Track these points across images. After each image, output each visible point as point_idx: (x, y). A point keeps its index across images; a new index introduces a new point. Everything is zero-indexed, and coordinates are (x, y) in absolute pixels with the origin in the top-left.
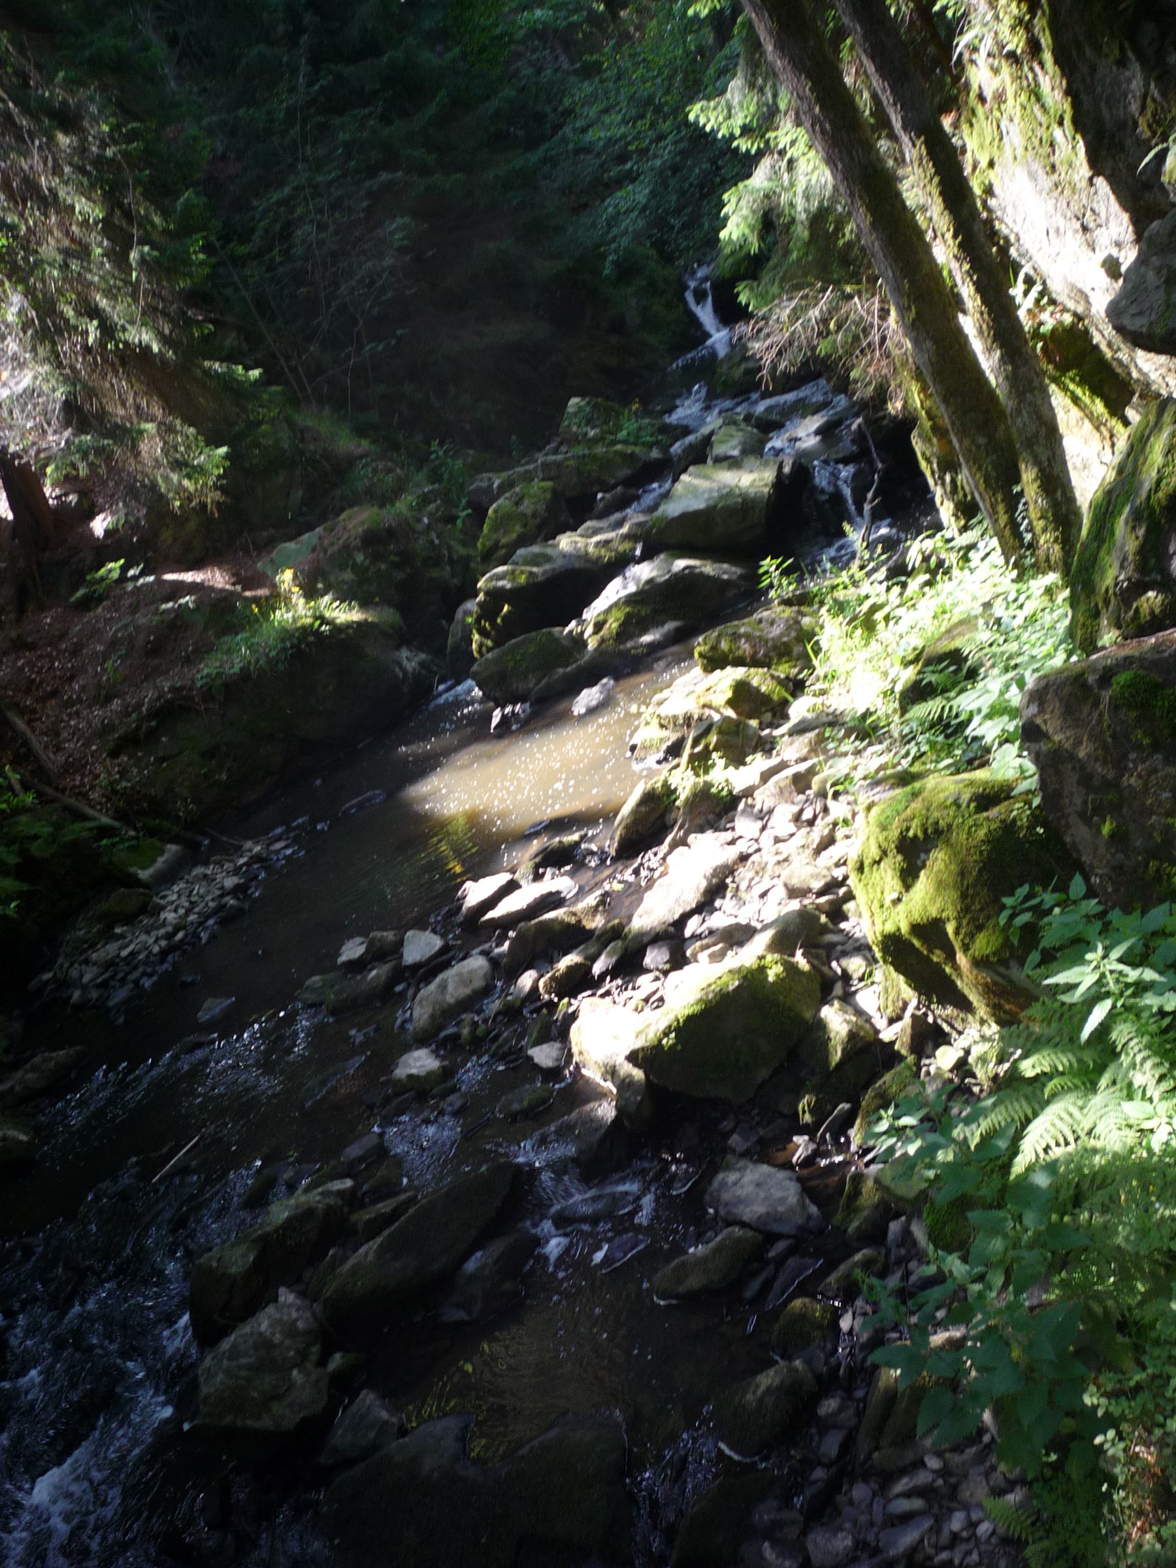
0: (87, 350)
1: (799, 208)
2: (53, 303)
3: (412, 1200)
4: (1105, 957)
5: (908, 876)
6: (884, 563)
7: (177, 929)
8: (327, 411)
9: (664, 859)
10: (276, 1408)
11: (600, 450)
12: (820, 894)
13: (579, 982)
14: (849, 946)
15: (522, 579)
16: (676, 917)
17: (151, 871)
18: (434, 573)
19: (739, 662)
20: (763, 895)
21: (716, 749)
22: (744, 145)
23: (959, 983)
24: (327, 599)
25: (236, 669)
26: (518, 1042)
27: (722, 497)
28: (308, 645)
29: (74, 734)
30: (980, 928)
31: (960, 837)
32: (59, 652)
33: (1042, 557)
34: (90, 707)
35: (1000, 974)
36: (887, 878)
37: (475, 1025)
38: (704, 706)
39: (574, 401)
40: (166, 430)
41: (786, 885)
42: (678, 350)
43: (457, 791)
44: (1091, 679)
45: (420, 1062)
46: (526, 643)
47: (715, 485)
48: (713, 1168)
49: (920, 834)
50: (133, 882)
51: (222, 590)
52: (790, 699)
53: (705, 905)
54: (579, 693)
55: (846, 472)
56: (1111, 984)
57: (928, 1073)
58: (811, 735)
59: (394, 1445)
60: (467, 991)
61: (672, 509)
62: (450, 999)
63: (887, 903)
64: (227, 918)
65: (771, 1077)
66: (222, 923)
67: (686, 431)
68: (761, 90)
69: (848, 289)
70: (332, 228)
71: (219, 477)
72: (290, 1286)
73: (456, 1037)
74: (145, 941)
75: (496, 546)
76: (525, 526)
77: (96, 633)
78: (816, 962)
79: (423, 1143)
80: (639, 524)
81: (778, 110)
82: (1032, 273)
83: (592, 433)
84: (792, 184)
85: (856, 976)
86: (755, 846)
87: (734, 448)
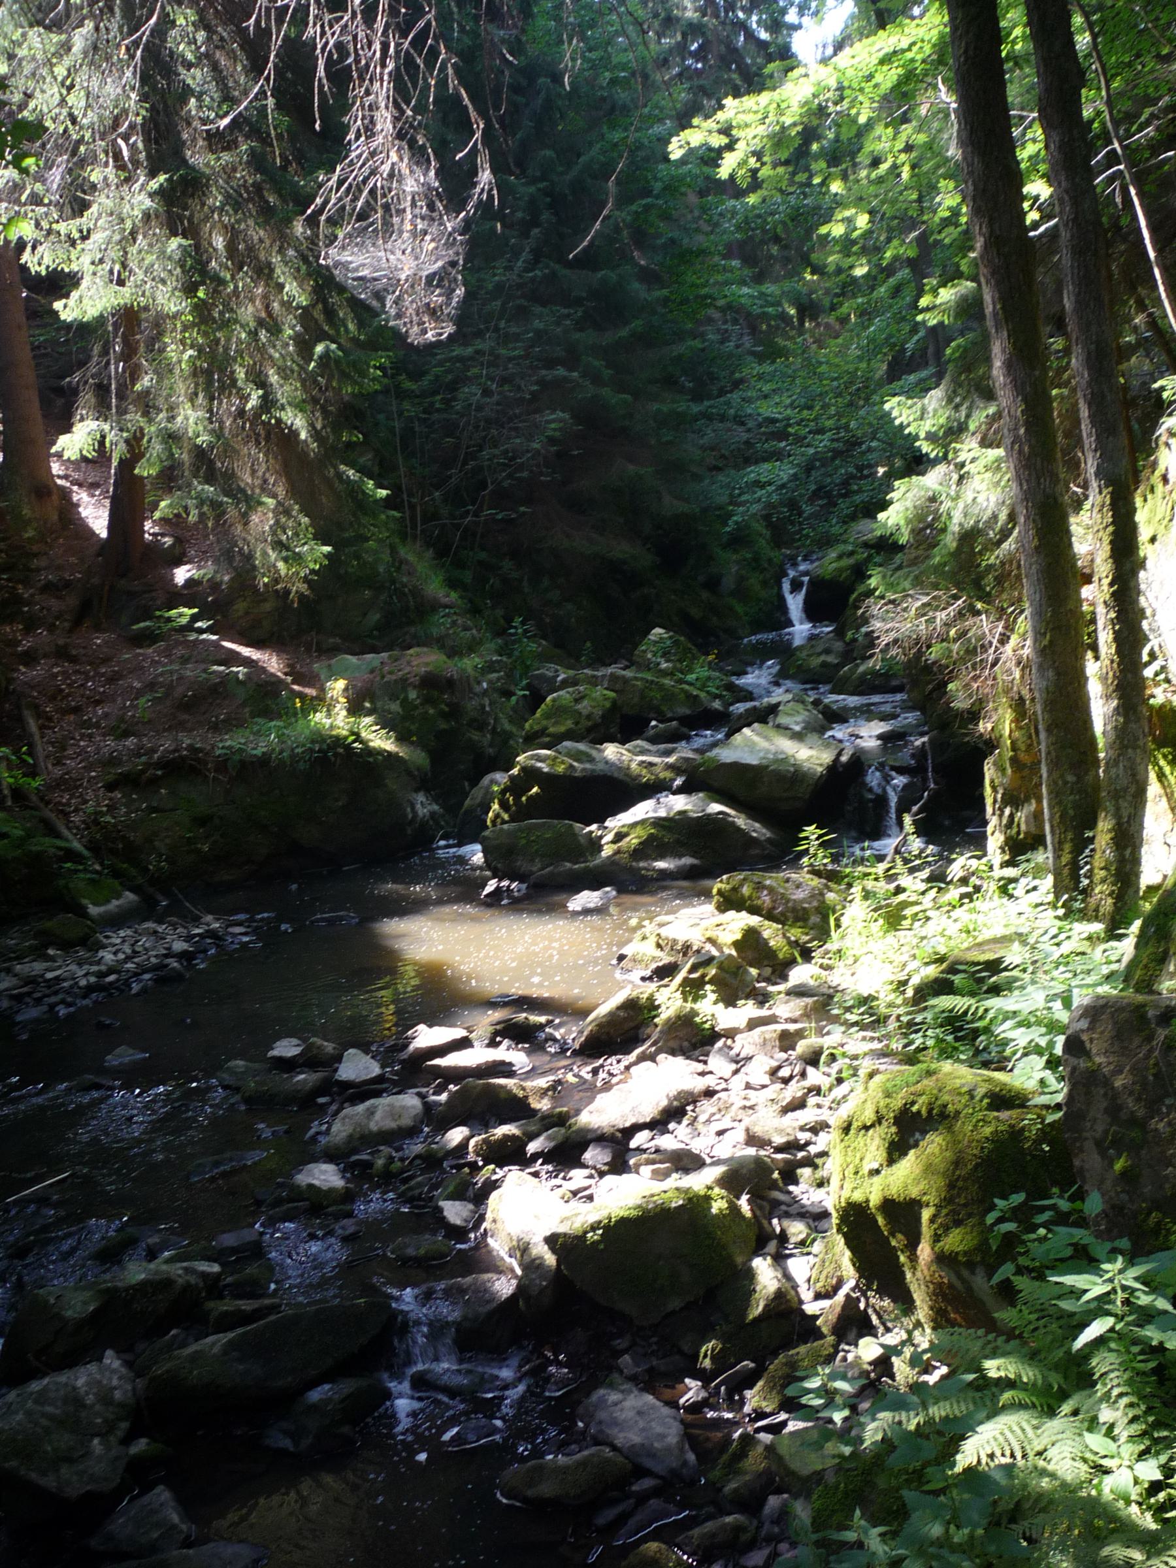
0: (241, 413)
1: (955, 520)
2: (228, 360)
3: (274, 1308)
4: (1121, 1272)
5: (896, 1151)
6: (929, 863)
7: (111, 971)
8: (430, 553)
9: (627, 1068)
10: (64, 1471)
11: (667, 682)
12: (778, 1150)
13: (510, 1154)
14: (793, 1209)
15: (561, 769)
16: (627, 1124)
17: (102, 909)
18: (475, 736)
19: (754, 911)
20: (720, 1133)
21: (711, 982)
22: (925, 447)
23: (909, 1276)
24: (368, 720)
25: (258, 752)
26: (430, 1191)
27: (776, 761)
28: (336, 755)
29: (79, 754)
30: (958, 1223)
31: (964, 1127)
32: (98, 674)
33: (1092, 905)
34: (104, 735)
35: (959, 1276)
36: (873, 1148)
37: (391, 1159)
38: (710, 940)
39: (658, 630)
40: (283, 510)
41: (747, 1130)
42: (758, 625)
43: (432, 939)
44: (1151, 1013)
45: (325, 1176)
46: (547, 828)
47: (773, 748)
48: (594, 1383)
49: (924, 1112)
50: (82, 912)
51: (273, 675)
52: (799, 959)
53: (659, 1124)
54: (578, 891)
55: (900, 781)
56: (1119, 1303)
57: (845, 1359)
58: (810, 1000)
59: (175, 1553)
60: (391, 1125)
61: (726, 755)
62: (373, 1127)
63: (865, 1171)
64: (164, 978)
65: (682, 1309)
66: (157, 981)
67: (748, 696)
68: (957, 408)
69: (979, 605)
70: (496, 397)
71: (313, 571)
72: (119, 1352)
73: (368, 1165)
74: (75, 971)
75: (543, 732)
76: (577, 723)
77: (138, 669)
78: (758, 1213)
79: (302, 1257)
80: (687, 760)
81: (967, 429)
82: (1156, 649)
83: (664, 665)
84: (958, 497)
85: (793, 1240)
86: (724, 1085)
87: (797, 723)
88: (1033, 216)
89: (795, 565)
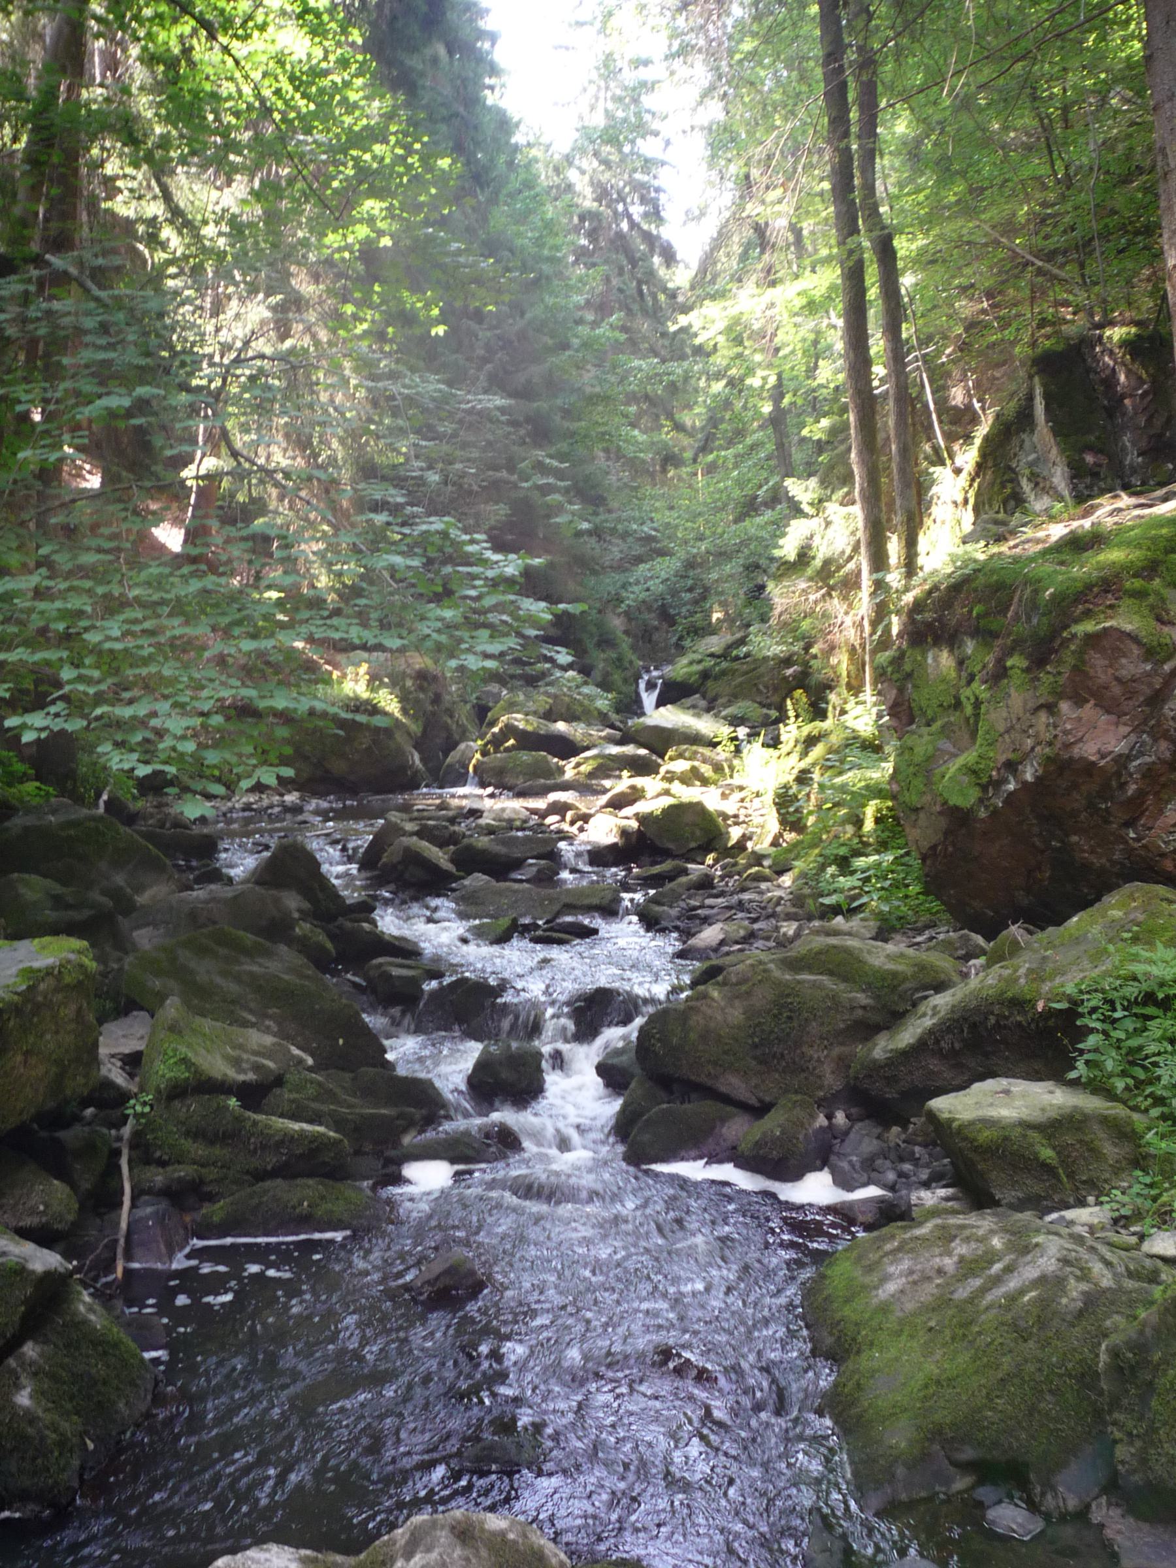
88: (876, 383)
89: (648, 671)
